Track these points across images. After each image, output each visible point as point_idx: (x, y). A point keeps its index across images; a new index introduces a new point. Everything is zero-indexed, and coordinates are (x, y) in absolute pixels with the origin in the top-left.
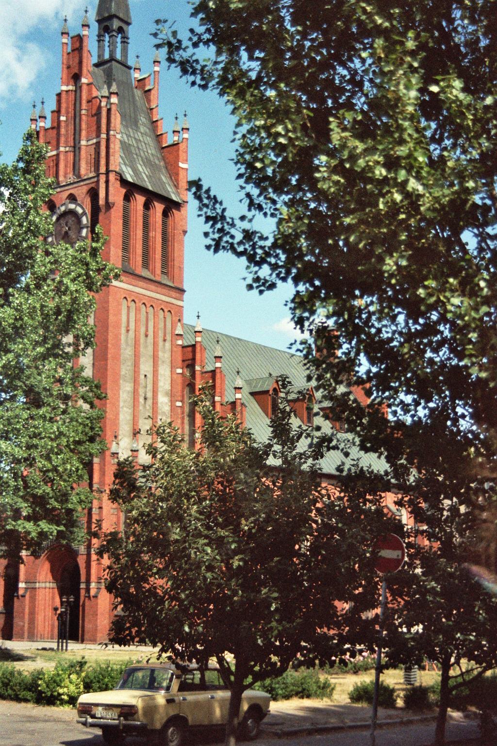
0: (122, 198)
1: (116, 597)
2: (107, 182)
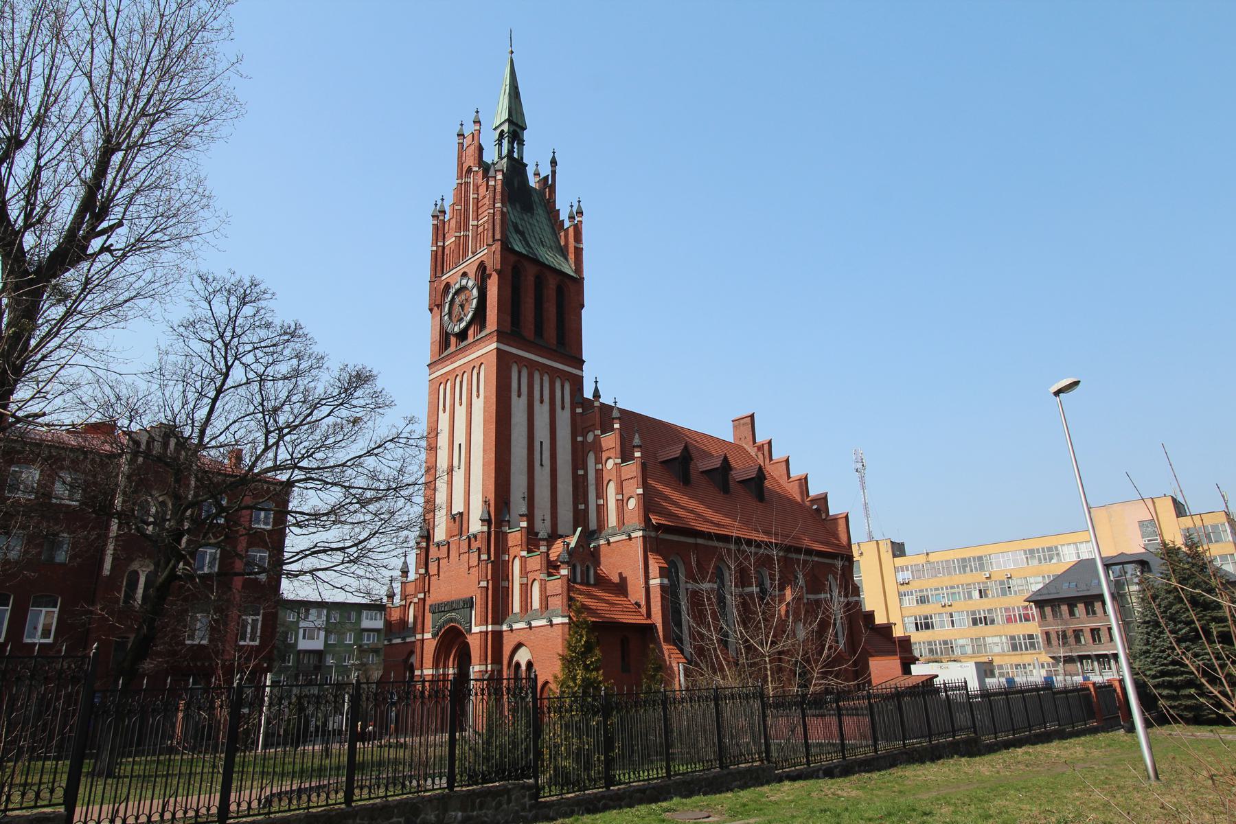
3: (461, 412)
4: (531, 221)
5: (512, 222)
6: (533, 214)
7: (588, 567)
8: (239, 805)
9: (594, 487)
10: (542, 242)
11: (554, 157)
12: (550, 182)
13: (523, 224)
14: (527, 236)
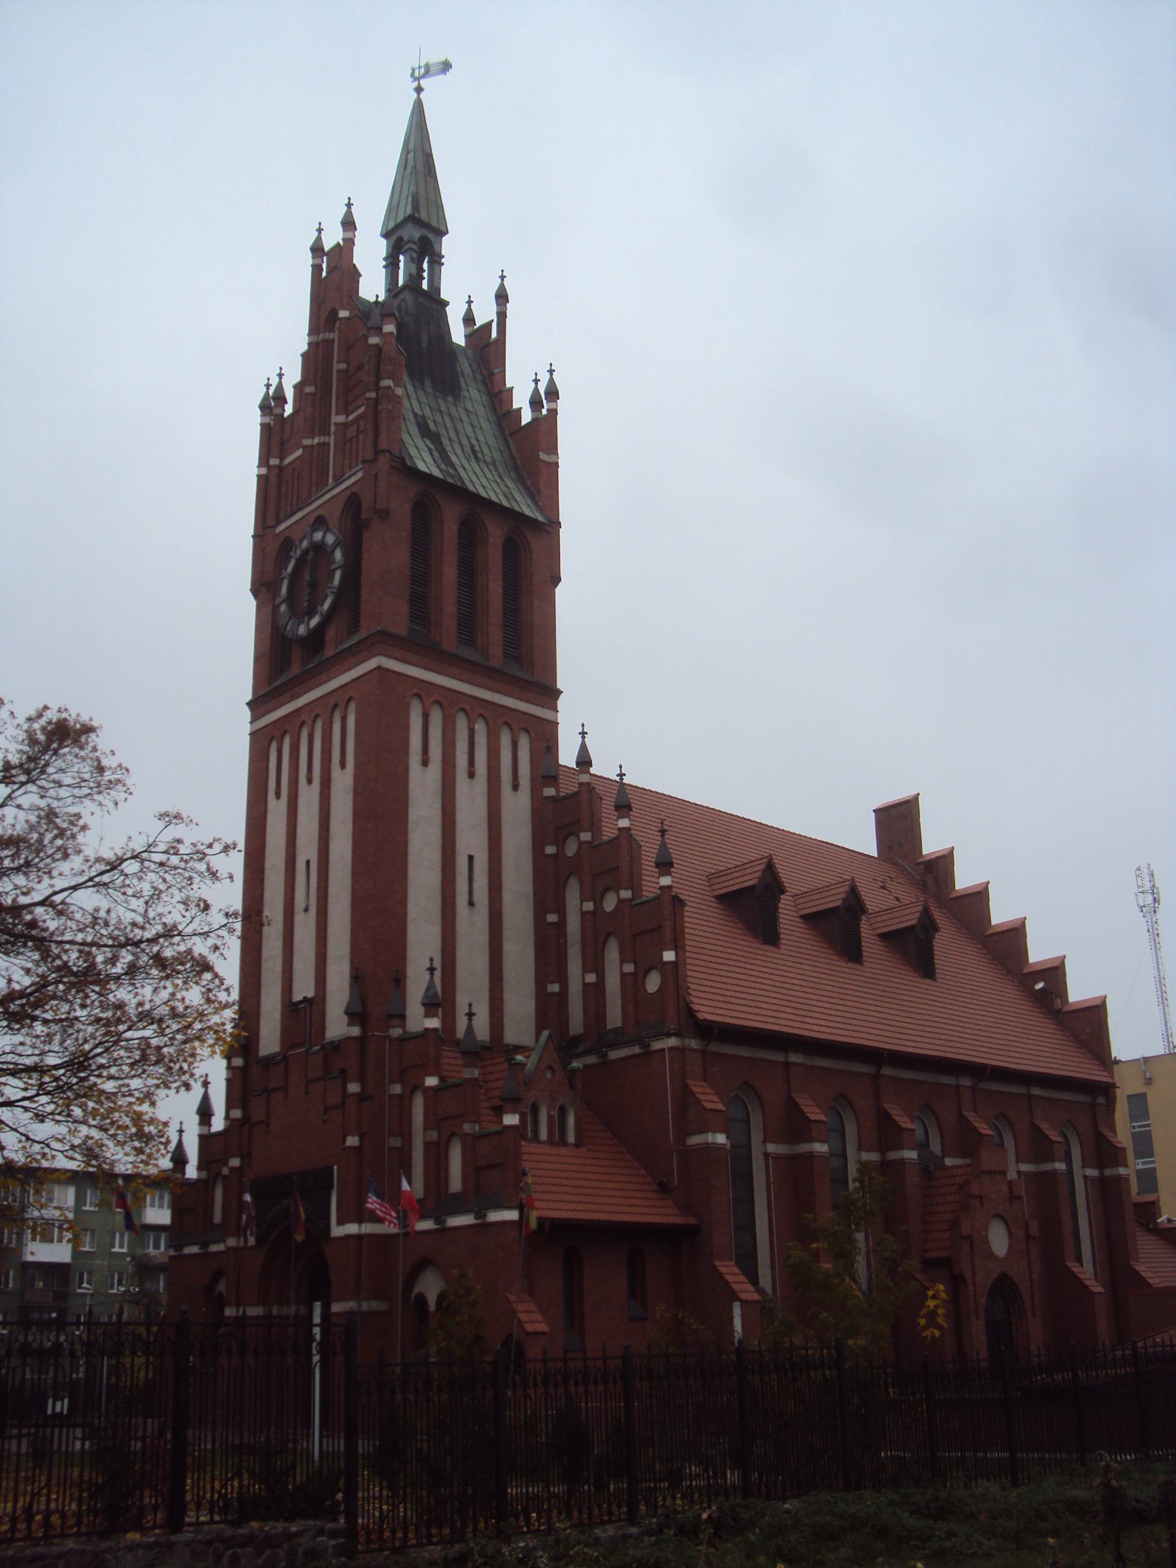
3: (309, 796)
4: (454, 412)
5: (415, 415)
7: (563, 1112)
10: (474, 452)
11: (502, 287)
12: (494, 335)
13: (438, 418)
14: (445, 441)
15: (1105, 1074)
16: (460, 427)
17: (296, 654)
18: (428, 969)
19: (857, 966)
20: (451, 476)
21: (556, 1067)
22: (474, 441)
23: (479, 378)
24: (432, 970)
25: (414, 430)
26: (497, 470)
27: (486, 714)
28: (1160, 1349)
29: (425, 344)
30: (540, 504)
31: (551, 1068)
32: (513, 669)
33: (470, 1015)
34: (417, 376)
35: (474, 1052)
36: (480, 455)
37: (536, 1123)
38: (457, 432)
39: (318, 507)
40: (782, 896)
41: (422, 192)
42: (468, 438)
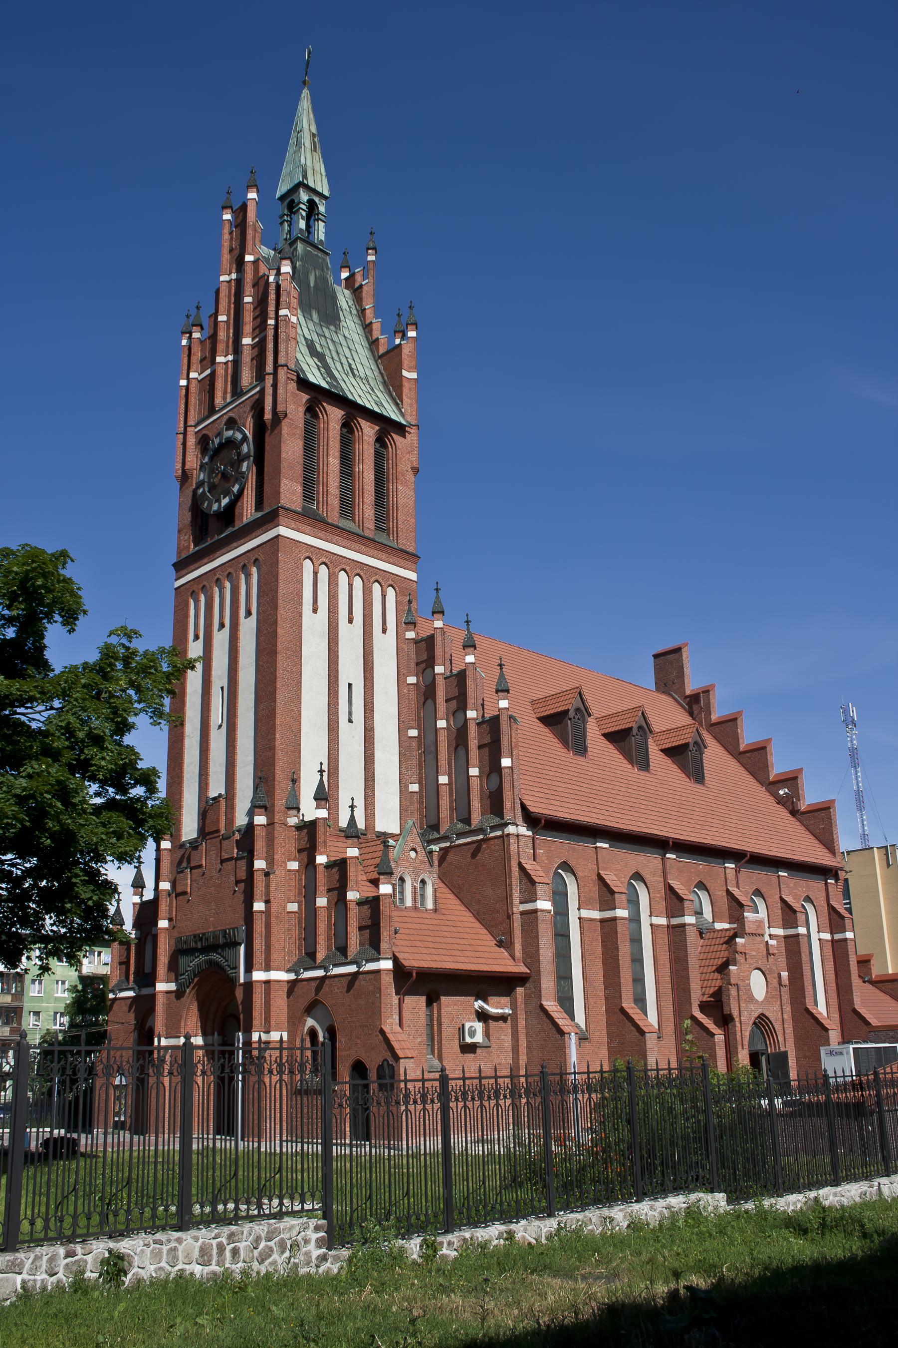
0: (302, 410)
1: (519, 1248)
2: (275, 386)
3: (221, 639)
4: (335, 339)
5: (306, 339)
6: (338, 328)
7: (423, 882)
8: (32, 1223)
9: (274, 302)
10: (352, 369)
14: (329, 360)
15: (833, 859)
16: (340, 350)
17: (213, 524)
18: (319, 771)
19: (646, 774)
20: (336, 387)
21: (418, 849)
22: (351, 361)
23: (354, 312)
24: (321, 772)
25: (305, 350)
26: (369, 384)
27: (362, 574)
28: (492, 1081)
29: (312, 284)
30: (403, 410)
31: (414, 850)
32: (382, 538)
33: (352, 807)
34: (306, 306)
35: (351, 833)
36: (356, 372)
37: (402, 892)
38: (338, 353)
39: (228, 412)
40: (589, 719)
41: (309, 164)
42: (347, 358)
